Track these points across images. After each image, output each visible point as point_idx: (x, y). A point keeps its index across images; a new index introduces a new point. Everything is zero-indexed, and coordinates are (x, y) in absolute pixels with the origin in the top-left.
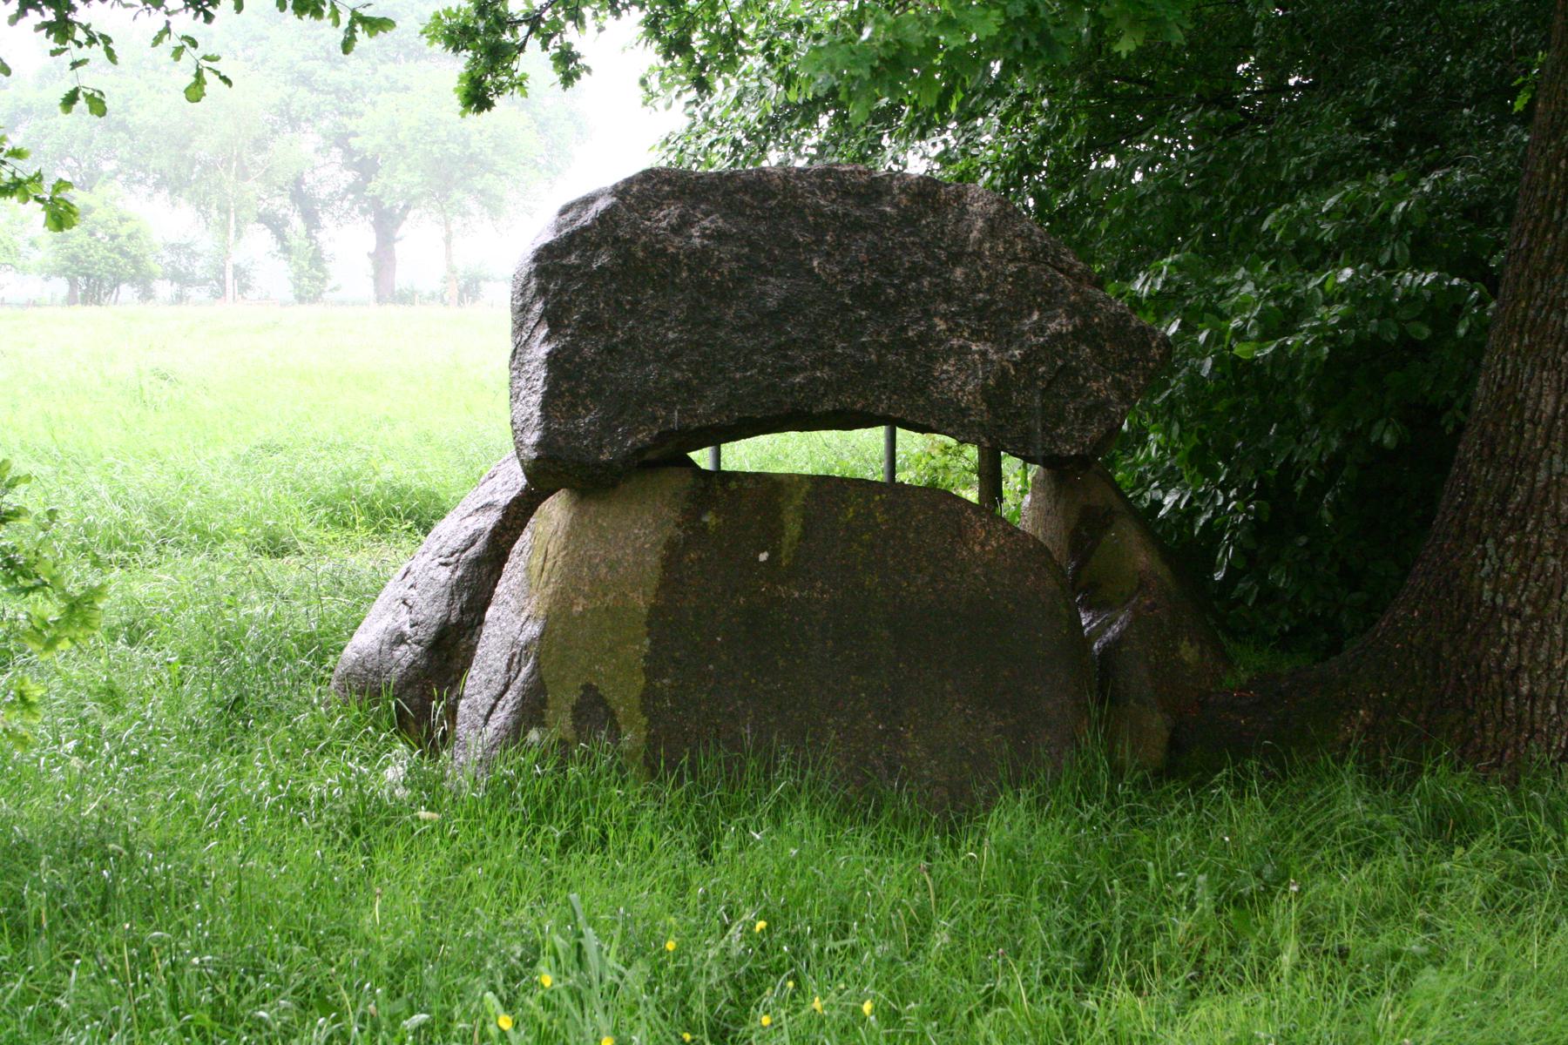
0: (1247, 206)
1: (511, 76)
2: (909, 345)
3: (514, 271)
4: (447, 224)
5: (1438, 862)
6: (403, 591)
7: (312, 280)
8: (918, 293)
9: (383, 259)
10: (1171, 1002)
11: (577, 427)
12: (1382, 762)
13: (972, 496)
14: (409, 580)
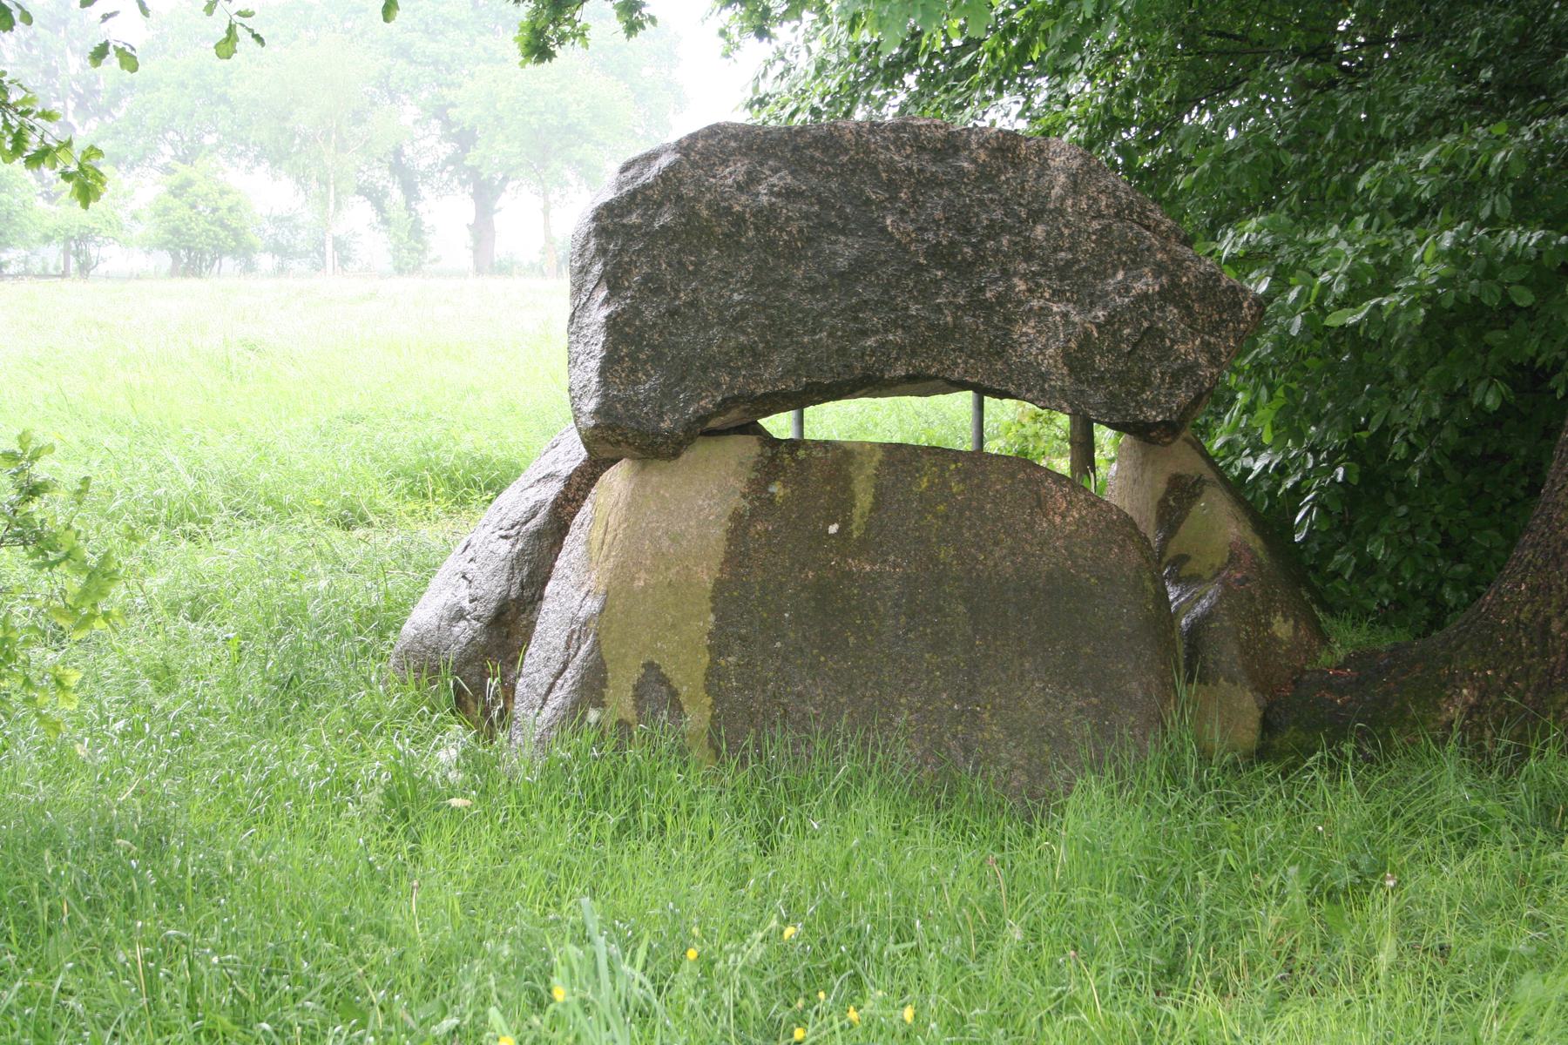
0: (1346, 163)
1: (574, 27)
2: (988, 307)
3: (571, 231)
4: (545, 195)
5: (1546, 853)
6: (464, 565)
7: (412, 247)
8: (997, 251)
9: (482, 230)
10: (1259, 1004)
11: (636, 394)
12: (1486, 743)
13: (1063, 466)
14: (470, 553)
